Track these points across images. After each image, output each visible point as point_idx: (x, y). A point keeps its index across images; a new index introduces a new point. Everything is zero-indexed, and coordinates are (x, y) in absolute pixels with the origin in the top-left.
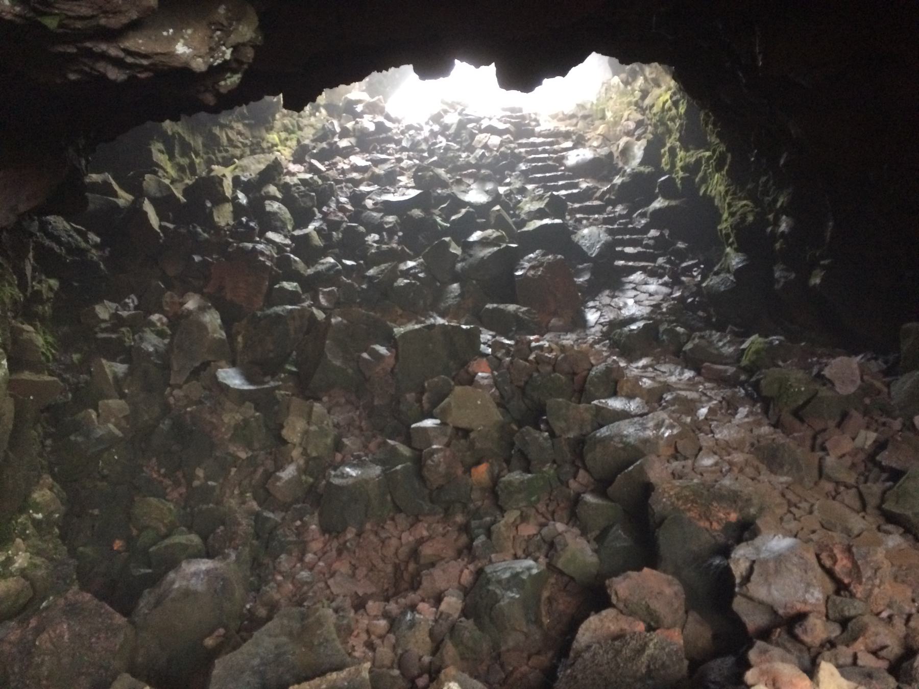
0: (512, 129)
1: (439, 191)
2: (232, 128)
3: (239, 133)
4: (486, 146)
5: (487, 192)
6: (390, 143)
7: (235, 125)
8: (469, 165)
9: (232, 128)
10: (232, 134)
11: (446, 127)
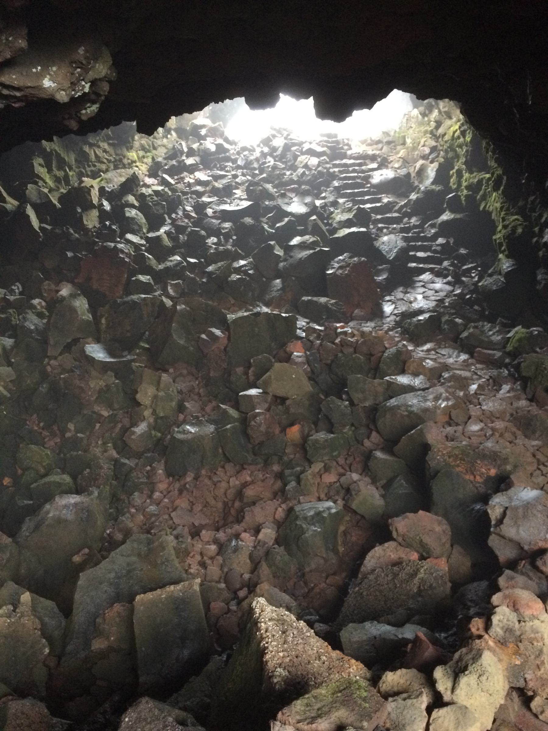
0: (328, 152)
1: (267, 203)
2: (99, 147)
3: (105, 151)
4: (306, 166)
5: (306, 204)
6: (228, 162)
7: (101, 144)
8: (292, 182)
9: (99, 147)
10: (99, 152)
11: (274, 149)
